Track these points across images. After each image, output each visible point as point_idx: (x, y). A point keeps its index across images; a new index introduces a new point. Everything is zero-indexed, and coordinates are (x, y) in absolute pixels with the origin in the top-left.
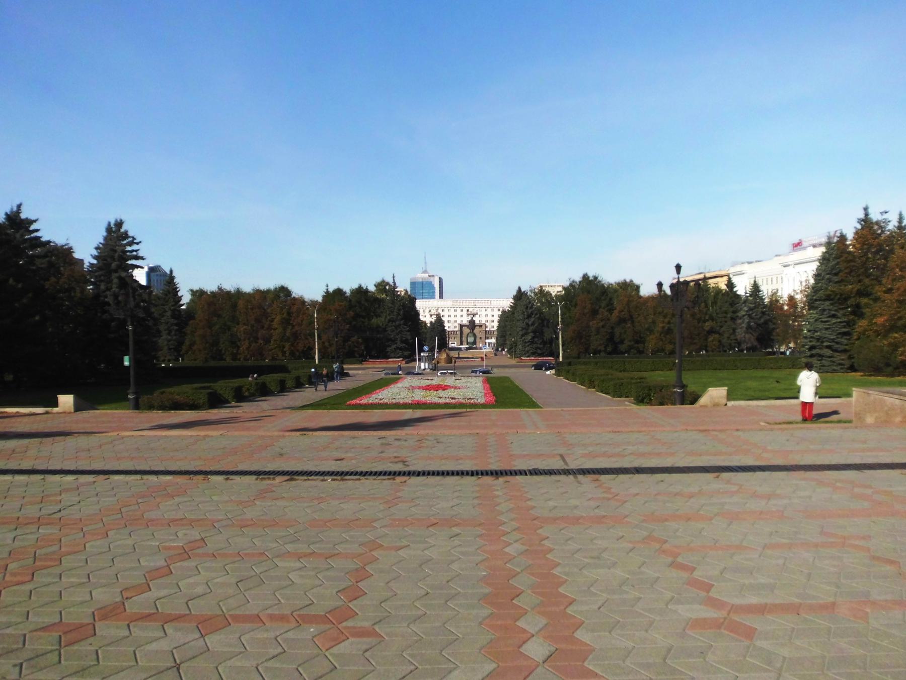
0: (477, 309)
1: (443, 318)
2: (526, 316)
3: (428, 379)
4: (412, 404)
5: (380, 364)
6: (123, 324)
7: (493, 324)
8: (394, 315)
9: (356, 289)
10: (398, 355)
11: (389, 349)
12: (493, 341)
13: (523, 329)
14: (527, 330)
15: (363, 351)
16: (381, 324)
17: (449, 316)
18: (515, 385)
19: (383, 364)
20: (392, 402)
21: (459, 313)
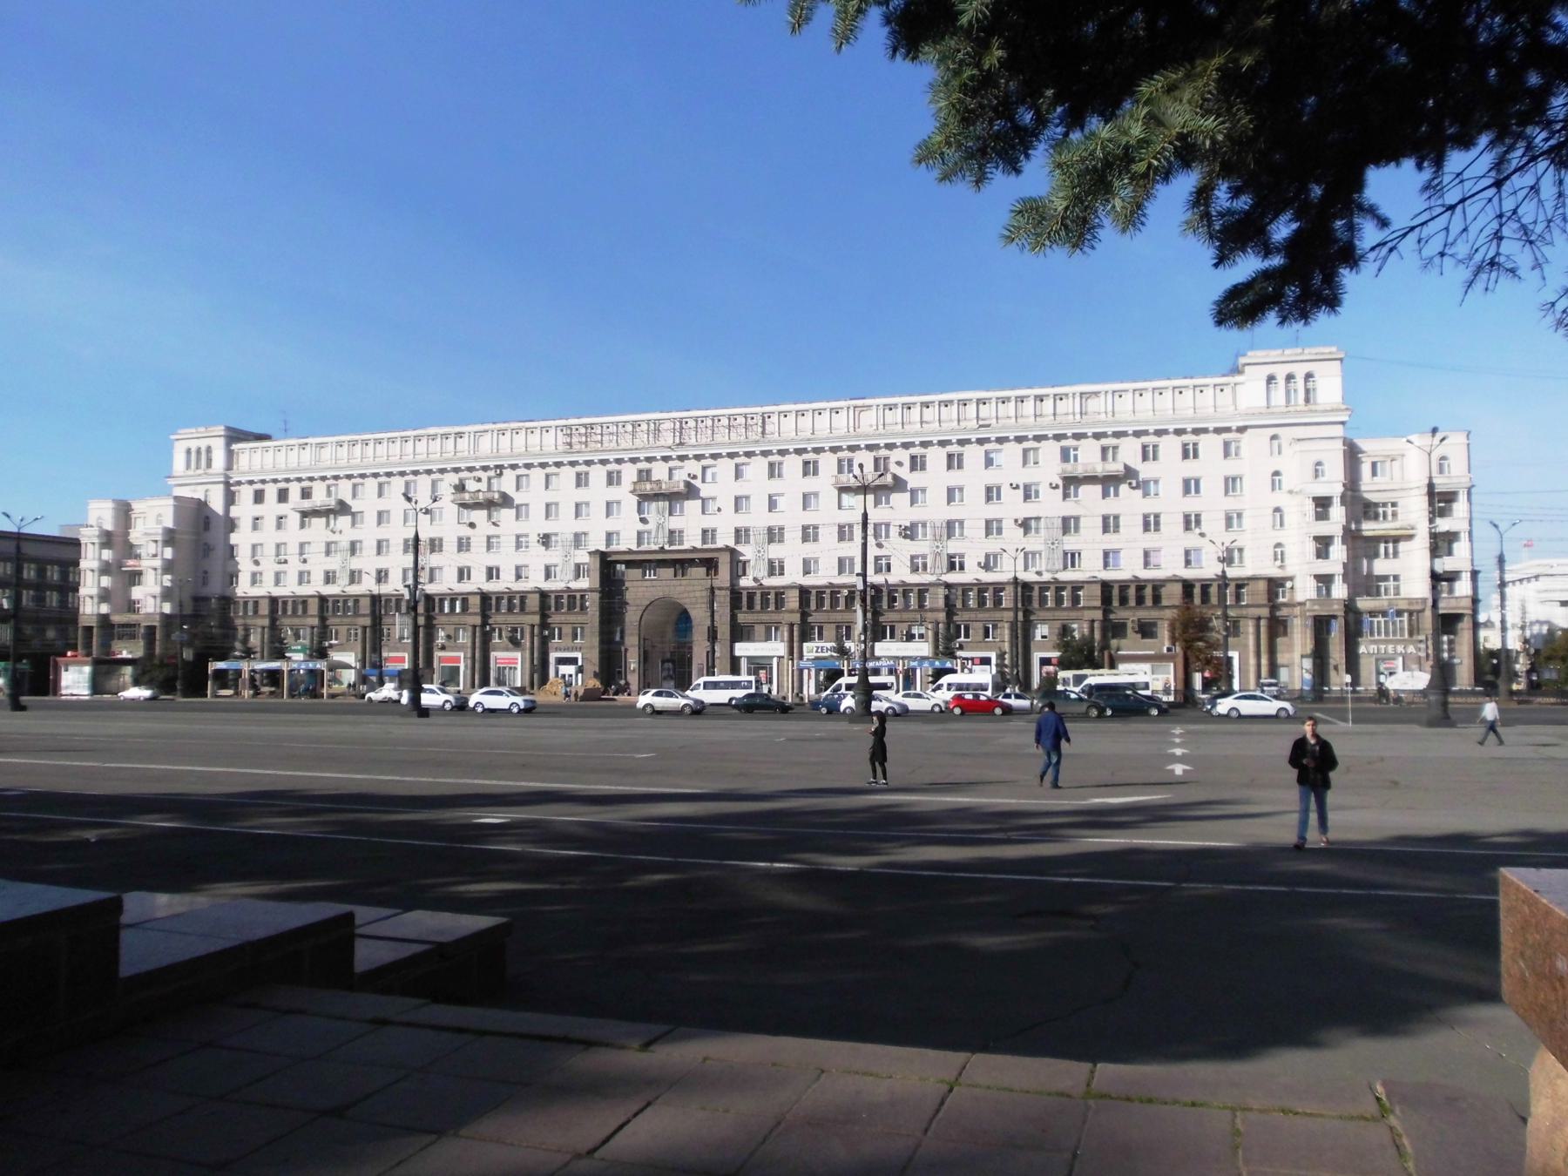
7: (775, 551)
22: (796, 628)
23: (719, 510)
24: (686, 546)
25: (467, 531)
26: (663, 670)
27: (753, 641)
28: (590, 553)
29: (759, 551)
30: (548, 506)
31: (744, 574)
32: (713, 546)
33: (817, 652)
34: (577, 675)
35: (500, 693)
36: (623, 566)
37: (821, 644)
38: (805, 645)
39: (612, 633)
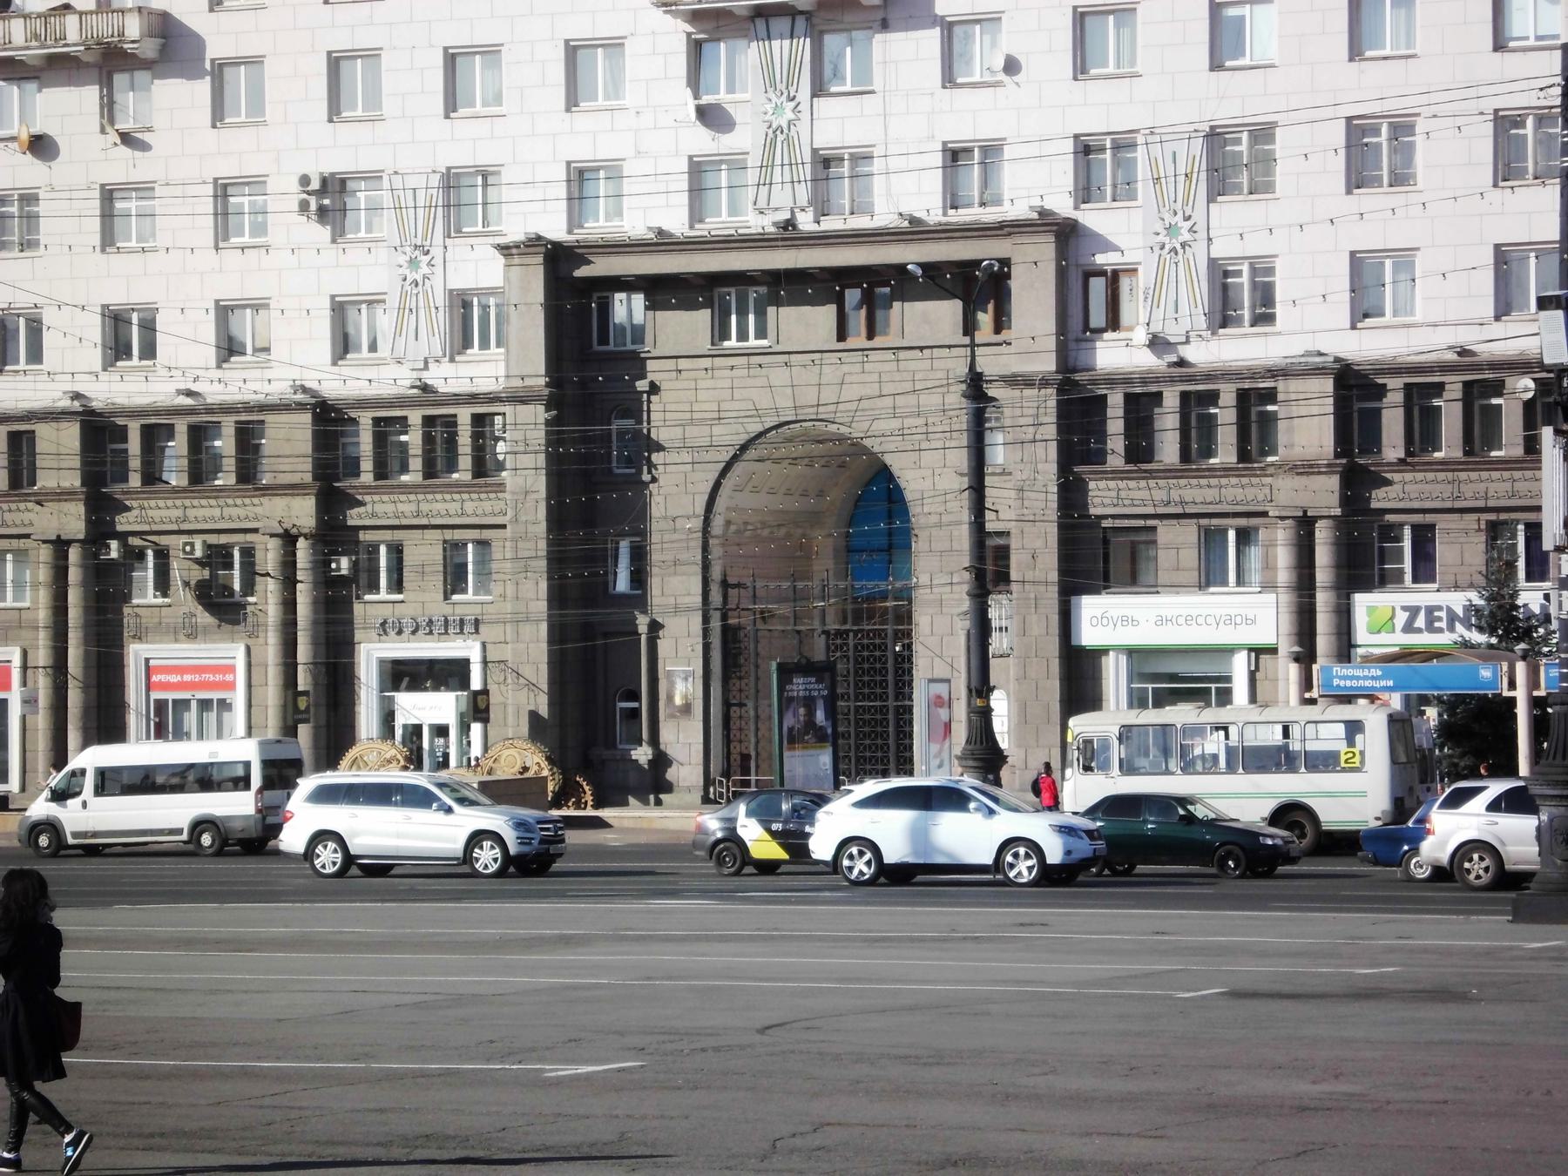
22: (1323, 535)
23: (1011, 66)
24: (884, 216)
25: (22, 171)
26: (785, 703)
27: (1154, 588)
28: (505, 250)
29: (1170, 229)
30: (335, 63)
31: (1114, 323)
33: (1409, 628)
34: (465, 729)
35: (418, 798)
36: (638, 300)
37: (1426, 596)
38: (1361, 601)
39: (606, 559)
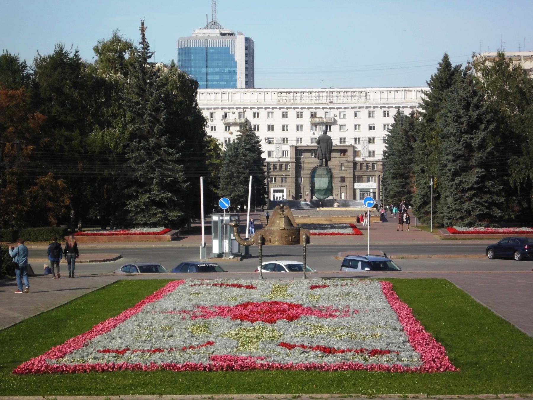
0: (335, 112)
1: (257, 133)
2: (464, 127)
3: (240, 286)
4: (210, 370)
5: (110, 241)
6: (132, 193)
7: (371, 147)
8: (144, 123)
9: (51, 58)
10: (154, 220)
11: (131, 204)
12: (372, 185)
13: (457, 157)
14: (467, 160)
15: (68, 208)
16: (112, 145)
17: (271, 128)
18: (477, 306)
19: (119, 240)
20: (153, 364)
21: (292, 121)
28: (290, 146)
32: (344, 144)
